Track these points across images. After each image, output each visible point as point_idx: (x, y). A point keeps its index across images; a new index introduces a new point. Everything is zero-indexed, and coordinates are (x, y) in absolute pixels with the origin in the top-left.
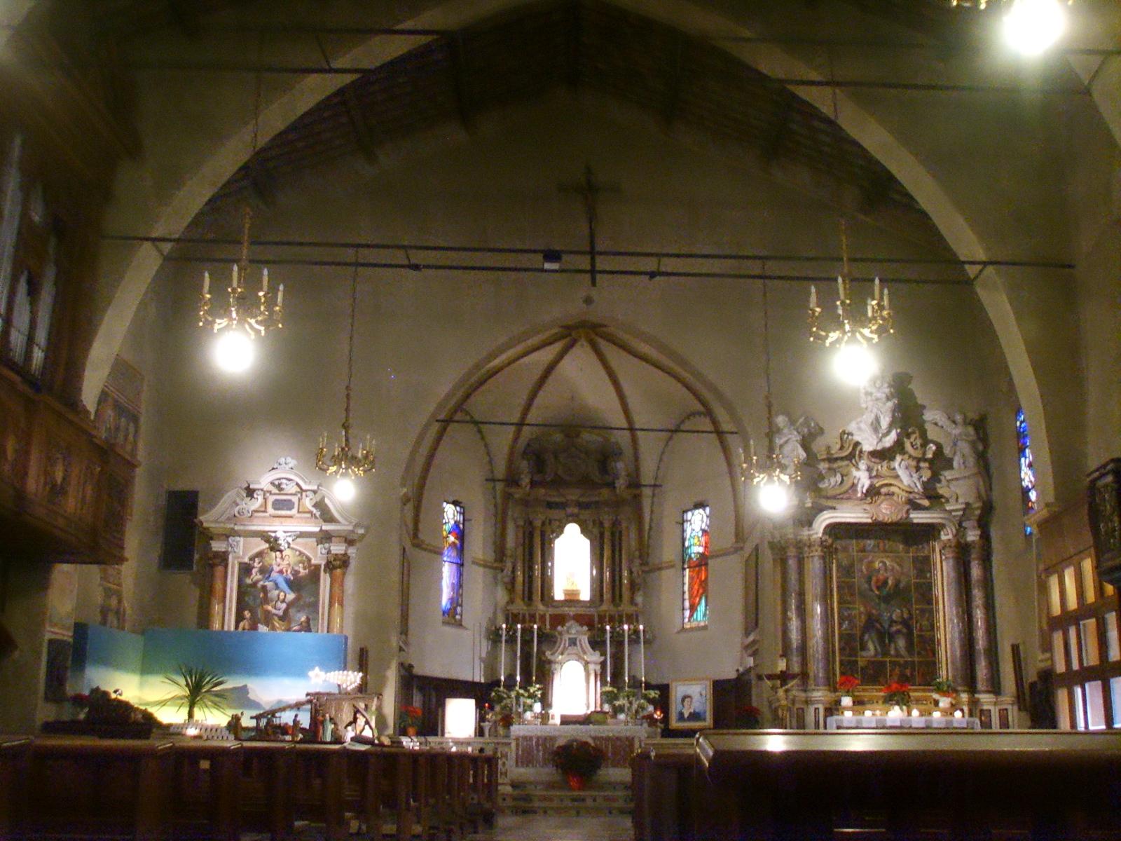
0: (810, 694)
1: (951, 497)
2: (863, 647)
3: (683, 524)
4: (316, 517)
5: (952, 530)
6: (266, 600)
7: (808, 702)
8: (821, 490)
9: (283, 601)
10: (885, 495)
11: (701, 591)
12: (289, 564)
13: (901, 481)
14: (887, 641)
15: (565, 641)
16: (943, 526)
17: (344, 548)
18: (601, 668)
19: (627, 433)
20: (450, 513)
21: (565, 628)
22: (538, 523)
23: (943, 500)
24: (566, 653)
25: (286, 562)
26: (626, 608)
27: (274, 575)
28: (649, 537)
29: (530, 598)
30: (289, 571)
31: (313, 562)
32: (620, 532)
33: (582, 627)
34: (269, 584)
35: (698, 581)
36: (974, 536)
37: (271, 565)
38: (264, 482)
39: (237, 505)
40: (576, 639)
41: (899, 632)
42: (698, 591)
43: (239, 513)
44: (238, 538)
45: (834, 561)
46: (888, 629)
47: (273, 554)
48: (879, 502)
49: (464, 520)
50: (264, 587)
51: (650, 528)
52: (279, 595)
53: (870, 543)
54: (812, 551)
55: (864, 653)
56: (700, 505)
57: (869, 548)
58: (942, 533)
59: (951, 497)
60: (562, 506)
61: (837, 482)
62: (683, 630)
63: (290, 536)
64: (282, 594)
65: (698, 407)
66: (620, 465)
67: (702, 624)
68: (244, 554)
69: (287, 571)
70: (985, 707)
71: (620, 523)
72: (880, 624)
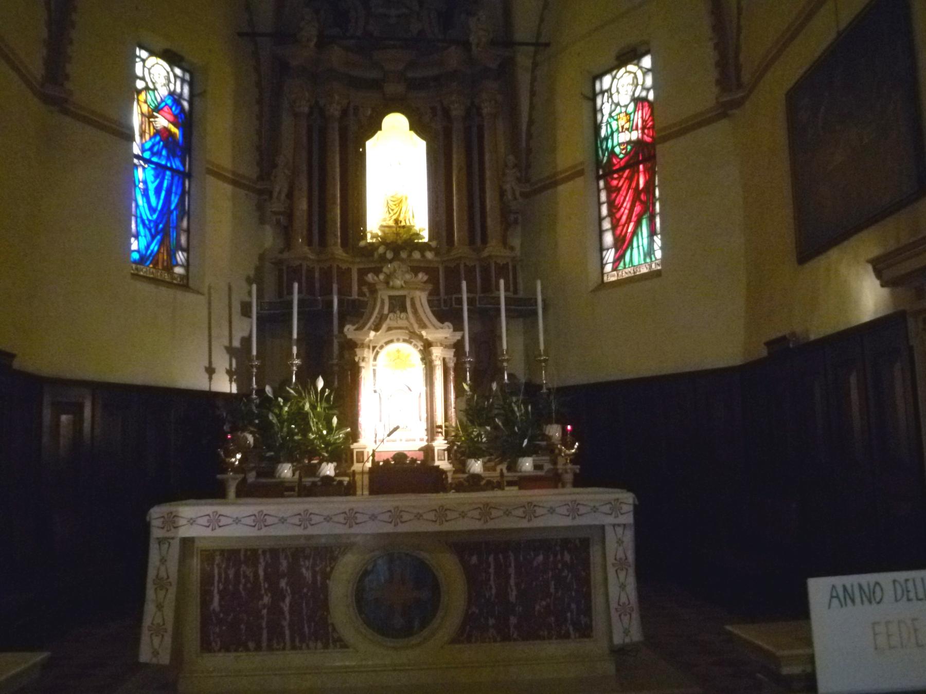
3: (594, 100)
11: (637, 209)
18: (456, 355)
21: (382, 277)
22: (335, 110)
24: (384, 327)
29: (323, 243)
32: (481, 128)
42: (631, 210)
51: (531, 122)
56: (629, 56)
62: (602, 285)
67: (644, 270)
71: (479, 109)
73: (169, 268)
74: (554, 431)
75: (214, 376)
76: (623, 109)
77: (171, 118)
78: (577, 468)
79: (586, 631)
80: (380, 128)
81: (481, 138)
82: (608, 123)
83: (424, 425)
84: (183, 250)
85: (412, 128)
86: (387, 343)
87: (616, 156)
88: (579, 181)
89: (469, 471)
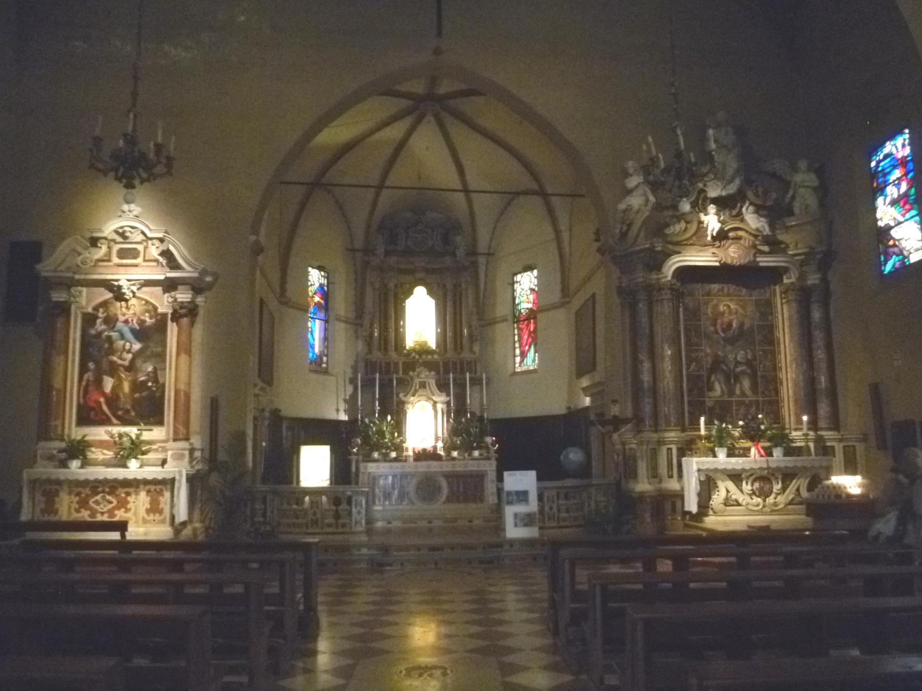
0: (662, 435)
1: (791, 243)
2: (711, 389)
3: (513, 286)
4: (162, 266)
5: (795, 274)
6: (112, 351)
7: (660, 442)
8: (667, 235)
9: (129, 351)
10: (733, 239)
12: (135, 314)
13: (748, 225)
14: (732, 380)
15: (416, 384)
16: (786, 270)
17: (190, 296)
19: (472, 186)
20: (316, 277)
21: (416, 373)
22: (391, 285)
23: (783, 246)
24: (417, 395)
25: (131, 312)
26: (466, 355)
27: (119, 325)
28: (484, 296)
29: (386, 349)
30: (135, 321)
31: (160, 310)
33: (430, 372)
34: (114, 335)
35: (527, 332)
36: (815, 279)
37: (116, 315)
38: (109, 229)
39: (80, 254)
40: (425, 382)
41: (743, 372)
42: (527, 340)
43: (82, 263)
44: (80, 288)
45: (681, 305)
46: (734, 370)
47: (118, 304)
48: (726, 246)
49: (328, 283)
50: (109, 338)
51: (485, 289)
52: (124, 346)
53: (715, 287)
54: (661, 295)
55: (711, 394)
57: (714, 292)
58: (785, 277)
59: (791, 243)
60: (412, 272)
61: (681, 229)
62: (515, 373)
63: (134, 285)
64: (128, 344)
65: (529, 184)
66: (458, 239)
67: (532, 368)
68: (87, 304)
69: (132, 321)
70: (828, 444)
71: (460, 285)
72: (727, 366)
73: (320, 365)
74: (489, 440)
75: (339, 413)
76: (525, 293)
77: (320, 296)
78: (497, 455)
79: (482, 501)
80: (412, 294)
81: (460, 299)
82: (519, 298)
83: (434, 437)
84: (325, 356)
85: (428, 294)
86: (418, 401)
87: (522, 313)
88: (505, 324)
89: (69, 436)
